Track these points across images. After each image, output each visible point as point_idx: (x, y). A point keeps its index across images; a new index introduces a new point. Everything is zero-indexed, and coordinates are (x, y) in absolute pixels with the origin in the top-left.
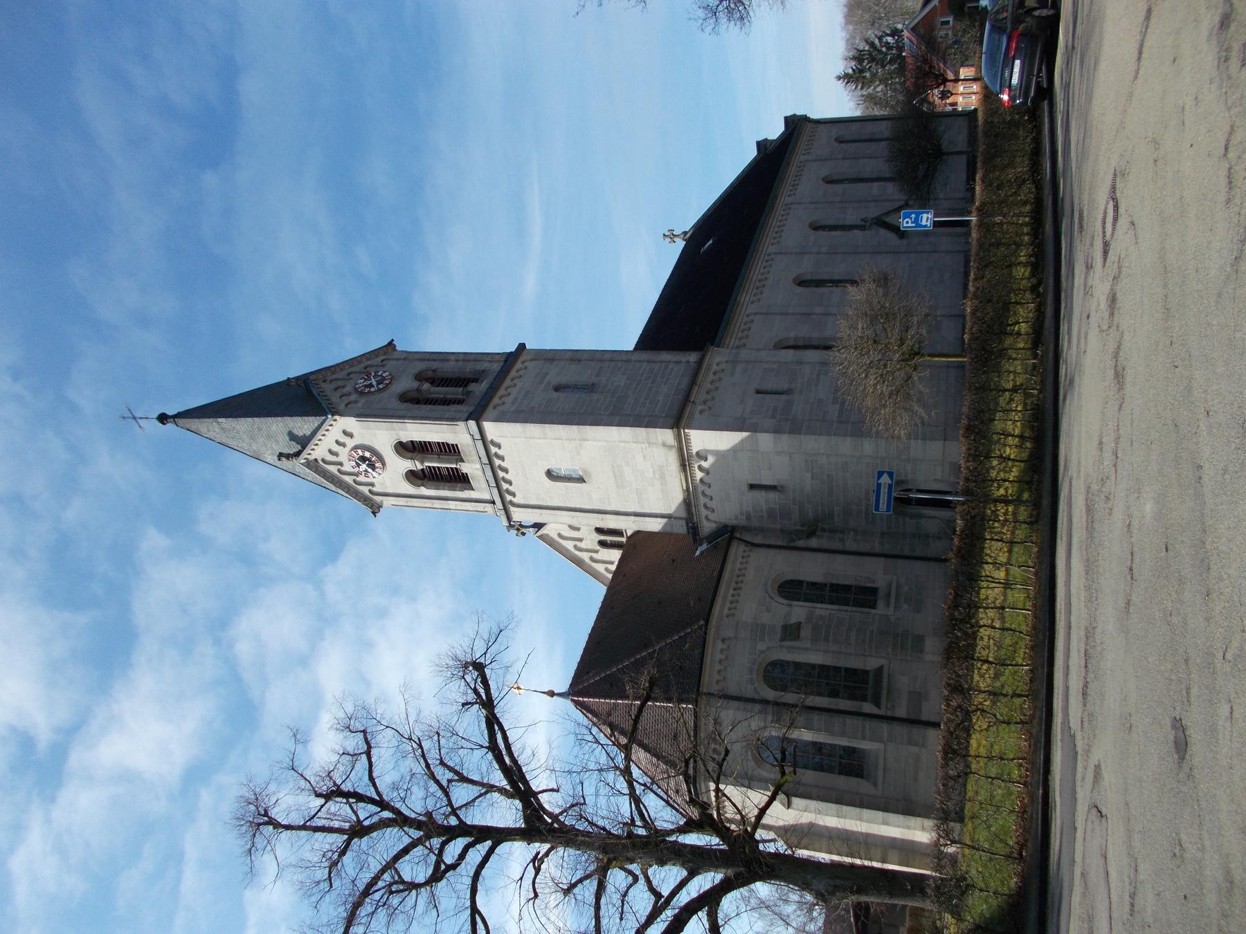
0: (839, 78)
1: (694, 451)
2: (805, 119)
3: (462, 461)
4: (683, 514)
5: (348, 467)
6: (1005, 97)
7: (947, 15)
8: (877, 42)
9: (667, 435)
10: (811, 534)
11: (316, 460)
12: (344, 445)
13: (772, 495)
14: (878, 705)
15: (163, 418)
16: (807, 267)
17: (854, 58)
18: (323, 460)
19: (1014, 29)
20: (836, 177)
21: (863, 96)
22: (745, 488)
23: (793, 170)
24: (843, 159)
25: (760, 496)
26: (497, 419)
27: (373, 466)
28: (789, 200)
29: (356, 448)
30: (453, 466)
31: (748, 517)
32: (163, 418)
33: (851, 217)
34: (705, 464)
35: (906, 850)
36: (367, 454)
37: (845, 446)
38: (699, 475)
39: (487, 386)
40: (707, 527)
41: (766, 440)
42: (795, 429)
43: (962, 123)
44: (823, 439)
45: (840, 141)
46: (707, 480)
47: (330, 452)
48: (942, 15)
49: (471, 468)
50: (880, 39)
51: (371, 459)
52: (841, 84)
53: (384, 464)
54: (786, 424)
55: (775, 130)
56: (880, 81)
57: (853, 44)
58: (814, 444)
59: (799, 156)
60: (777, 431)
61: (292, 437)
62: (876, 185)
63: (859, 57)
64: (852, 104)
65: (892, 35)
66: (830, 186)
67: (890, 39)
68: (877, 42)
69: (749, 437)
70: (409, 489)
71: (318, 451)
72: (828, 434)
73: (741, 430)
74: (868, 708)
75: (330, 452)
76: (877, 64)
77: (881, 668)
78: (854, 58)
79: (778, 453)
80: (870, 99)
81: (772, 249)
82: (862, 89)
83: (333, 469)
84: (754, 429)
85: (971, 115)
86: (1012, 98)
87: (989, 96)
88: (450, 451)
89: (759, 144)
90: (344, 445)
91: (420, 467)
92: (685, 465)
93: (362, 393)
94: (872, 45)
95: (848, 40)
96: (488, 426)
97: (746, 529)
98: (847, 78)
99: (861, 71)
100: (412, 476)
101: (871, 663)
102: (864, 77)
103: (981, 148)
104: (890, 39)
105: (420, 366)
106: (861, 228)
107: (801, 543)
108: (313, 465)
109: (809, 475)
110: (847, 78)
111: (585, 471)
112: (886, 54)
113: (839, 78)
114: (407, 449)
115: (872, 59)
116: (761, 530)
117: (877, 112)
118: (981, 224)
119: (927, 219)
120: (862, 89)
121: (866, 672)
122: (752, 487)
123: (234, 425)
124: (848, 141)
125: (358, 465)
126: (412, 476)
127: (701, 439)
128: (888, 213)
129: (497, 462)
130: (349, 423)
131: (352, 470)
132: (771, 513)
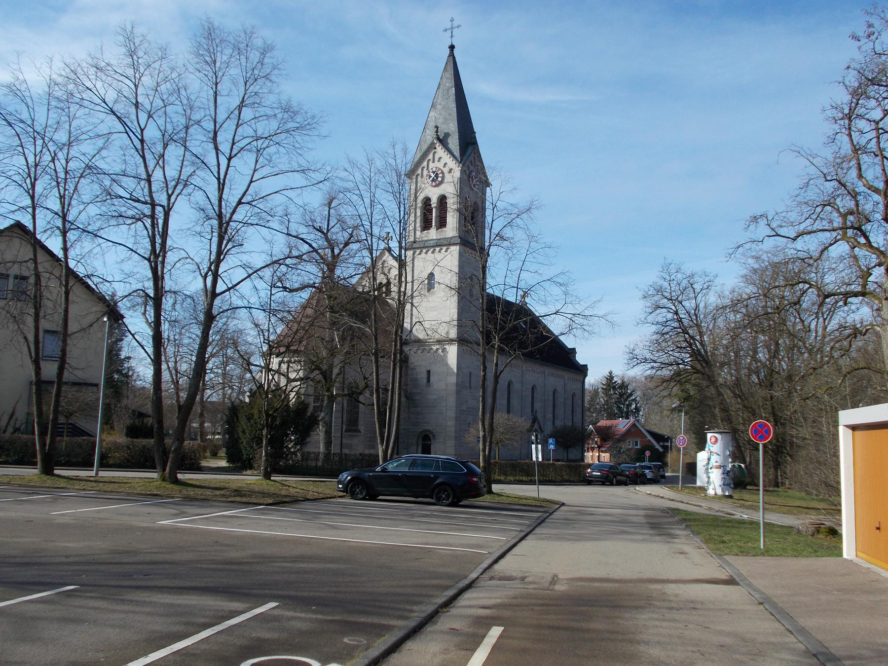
0: (611, 373)
1: (446, 347)
2: (585, 375)
3: (437, 230)
4: (413, 338)
5: (431, 165)
6: (589, 470)
7: (641, 445)
8: (633, 397)
9: (453, 334)
10: (406, 397)
11: (435, 148)
12: (444, 166)
13: (425, 381)
14: (346, 431)
15: (452, 47)
16: (516, 386)
17: (623, 383)
18: (435, 152)
19: (610, 472)
20: (556, 395)
21: (598, 389)
22: (428, 369)
23: (561, 373)
24: (565, 398)
25: (425, 375)
26: (461, 255)
27: (433, 180)
28: (547, 372)
29: (442, 173)
30: (433, 224)
31: (413, 369)
32: (452, 47)
33: (537, 405)
34: (440, 351)
35: (537, 458)
36: (440, 179)
37: (451, 413)
38: (435, 348)
39: (457, 215)
40: (406, 349)
41: (453, 380)
42: (458, 392)
43: (578, 457)
44: (454, 404)
45: (573, 395)
46: (432, 351)
47: (440, 158)
48: (641, 442)
49: (433, 234)
50: (634, 400)
51: (437, 179)
52: (607, 373)
53: (434, 186)
54: (460, 387)
55: (580, 359)
56: (607, 401)
57: (632, 382)
58: (452, 400)
59: (567, 375)
60: (457, 384)
61: (447, 135)
62: (552, 416)
63: (623, 386)
64: (592, 381)
65: (636, 408)
66: (552, 393)
67: (633, 406)
68: (633, 397)
69: (454, 372)
70: (421, 197)
71: (440, 151)
72: (456, 407)
73: (457, 369)
74: (344, 427)
75: (440, 158)
76: (618, 398)
77: (360, 432)
78: (623, 383)
79: (446, 385)
80: (596, 392)
81: (524, 368)
82: (603, 389)
83: (430, 156)
84: (458, 374)
85: (582, 459)
86: (588, 473)
87: (589, 466)
88: (442, 223)
89: (574, 349)
90: (444, 166)
91: (433, 206)
92: (439, 342)
93: (469, 177)
94: (631, 395)
95: (635, 378)
96: (457, 248)
97: (407, 367)
98: (610, 378)
99: (614, 388)
100: (427, 201)
101: (361, 428)
102: (610, 390)
103: (572, 464)
104: (633, 406)
105: (480, 203)
106: (532, 411)
107: (402, 393)
108: (432, 147)
109: (435, 397)
110: (610, 378)
111: (434, 293)
112: (624, 404)
113: (611, 373)
114: (443, 199)
115: (621, 395)
116: (406, 375)
117: (587, 398)
118: (550, 464)
119: (552, 447)
120: (603, 389)
121: (357, 426)
122: (429, 372)
123: (451, 97)
124: (573, 399)
125: (434, 172)
126: (427, 201)
127: (452, 352)
128: (539, 423)
129: (438, 249)
130: (457, 173)
131: (430, 168)
132: (416, 380)
